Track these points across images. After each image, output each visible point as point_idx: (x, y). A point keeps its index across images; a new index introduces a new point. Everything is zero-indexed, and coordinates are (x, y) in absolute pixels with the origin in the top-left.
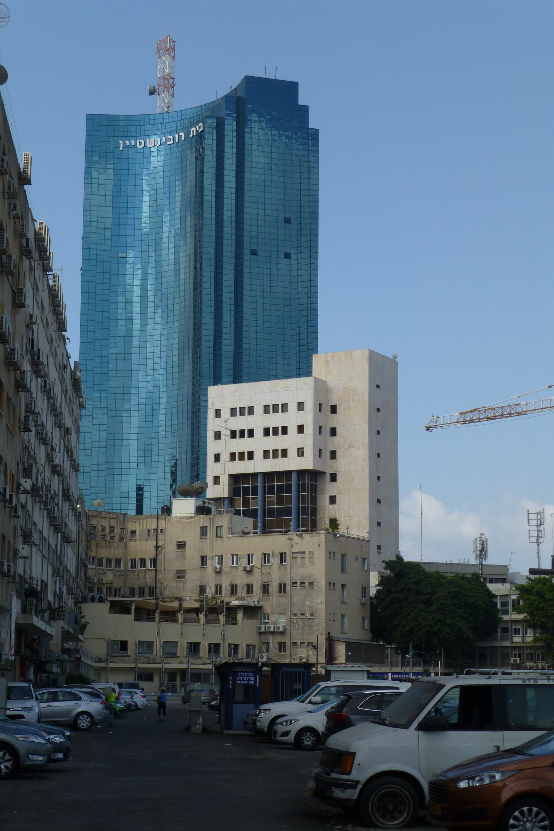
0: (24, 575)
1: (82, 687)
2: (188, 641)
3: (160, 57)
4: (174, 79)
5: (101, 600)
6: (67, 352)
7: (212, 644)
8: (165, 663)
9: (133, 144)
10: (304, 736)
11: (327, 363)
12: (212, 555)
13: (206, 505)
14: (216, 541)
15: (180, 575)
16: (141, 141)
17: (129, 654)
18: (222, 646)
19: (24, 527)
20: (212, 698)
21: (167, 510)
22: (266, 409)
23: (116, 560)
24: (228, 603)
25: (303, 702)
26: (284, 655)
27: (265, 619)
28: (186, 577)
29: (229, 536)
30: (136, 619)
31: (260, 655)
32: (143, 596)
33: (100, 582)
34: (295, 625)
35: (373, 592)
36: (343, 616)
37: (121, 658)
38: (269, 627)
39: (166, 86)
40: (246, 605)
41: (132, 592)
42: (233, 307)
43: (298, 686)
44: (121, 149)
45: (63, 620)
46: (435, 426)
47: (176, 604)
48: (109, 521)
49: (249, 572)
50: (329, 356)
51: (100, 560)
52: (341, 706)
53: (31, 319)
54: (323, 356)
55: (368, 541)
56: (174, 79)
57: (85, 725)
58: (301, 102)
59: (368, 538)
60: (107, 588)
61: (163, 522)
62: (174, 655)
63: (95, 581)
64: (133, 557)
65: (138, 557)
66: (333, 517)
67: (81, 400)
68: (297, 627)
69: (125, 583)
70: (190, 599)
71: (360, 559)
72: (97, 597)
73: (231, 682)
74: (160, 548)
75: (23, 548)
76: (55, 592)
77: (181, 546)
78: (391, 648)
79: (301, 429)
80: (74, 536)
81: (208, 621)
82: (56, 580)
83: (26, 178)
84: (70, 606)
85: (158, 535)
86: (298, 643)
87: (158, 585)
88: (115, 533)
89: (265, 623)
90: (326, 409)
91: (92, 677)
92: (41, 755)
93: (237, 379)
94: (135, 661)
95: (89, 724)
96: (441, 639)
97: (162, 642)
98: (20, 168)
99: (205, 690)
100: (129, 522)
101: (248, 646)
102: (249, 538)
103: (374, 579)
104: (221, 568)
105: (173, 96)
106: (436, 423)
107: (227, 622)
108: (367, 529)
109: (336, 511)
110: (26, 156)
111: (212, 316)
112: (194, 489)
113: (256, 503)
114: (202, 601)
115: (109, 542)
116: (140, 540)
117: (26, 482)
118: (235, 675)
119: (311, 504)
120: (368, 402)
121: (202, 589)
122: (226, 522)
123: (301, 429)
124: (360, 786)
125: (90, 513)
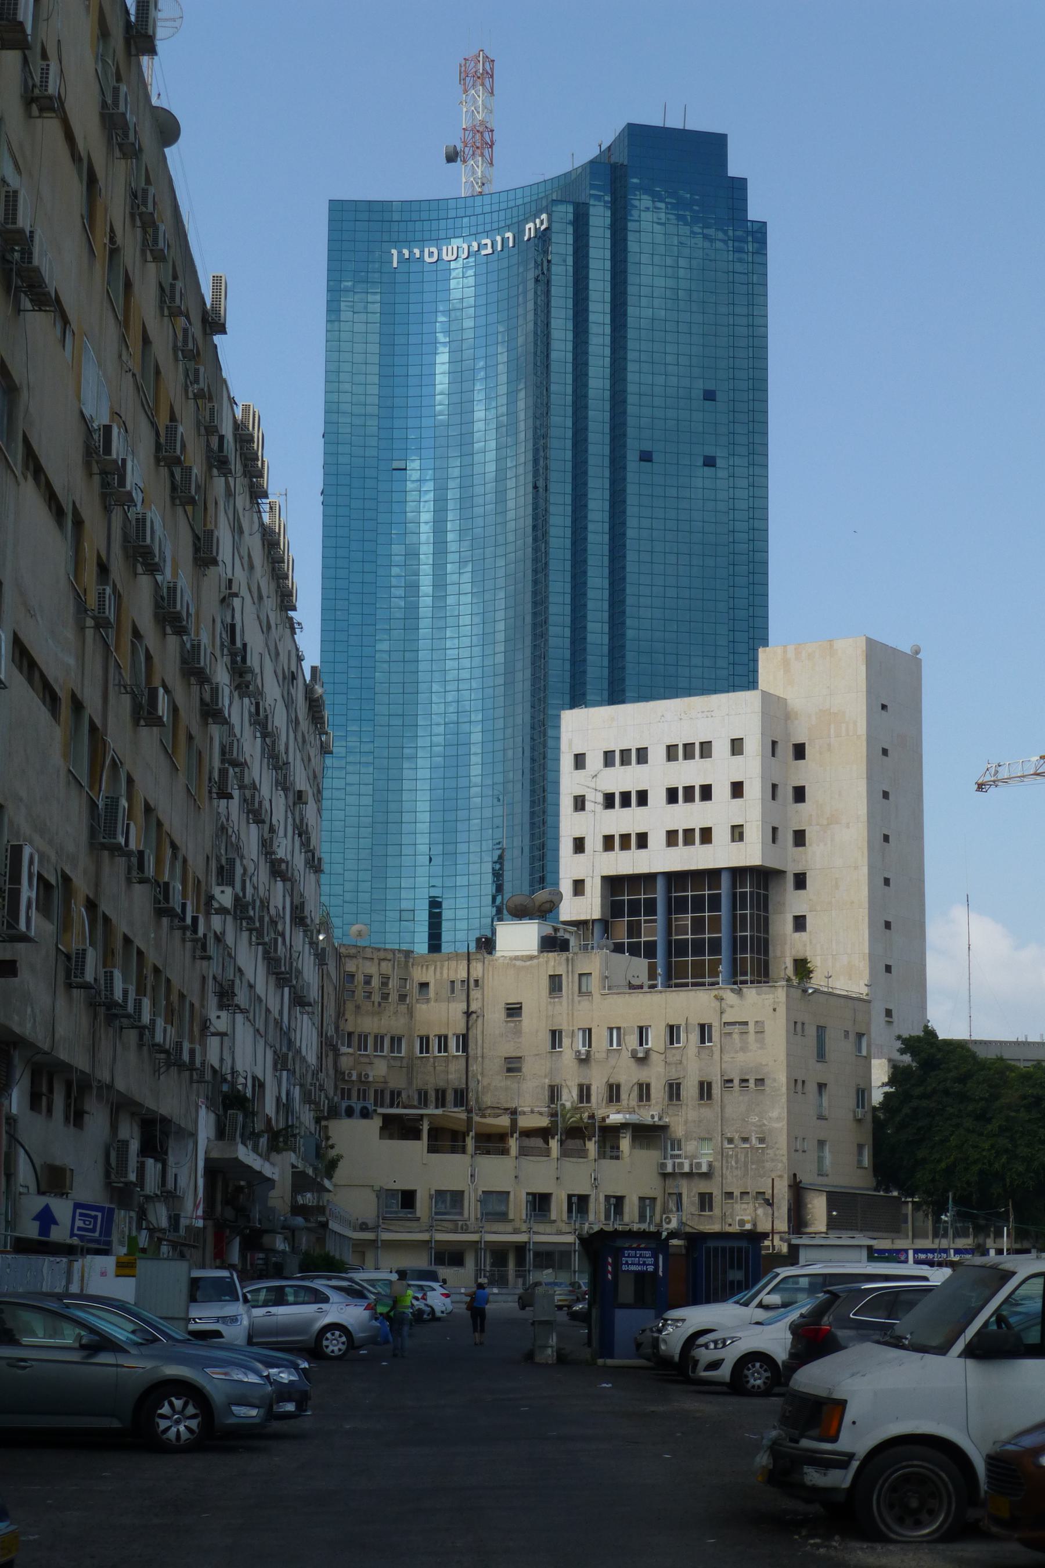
0: (221, 1067)
1: (329, 1278)
2: (530, 1191)
3: (466, 91)
4: (492, 131)
5: (365, 1114)
6: (297, 649)
7: (574, 1195)
8: (486, 1232)
9: (418, 256)
10: (749, 1369)
11: (786, 663)
12: (571, 1029)
13: (559, 934)
14: (579, 1002)
15: (513, 1066)
16: (432, 249)
17: (418, 1215)
18: (592, 1200)
19: (219, 978)
20: (575, 1298)
21: (487, 944)
22: (671, 752)
23: (392, 1039)
24: (604, 1119)
25: (746, 1304)
26: (710, 1217)
27: (673, 1149)
28: (524, 1070)
29: (603, 992)
30: (432, 1150)
31: (664, 1216)
32: (443, 1105)
33: (363, 1080)
34: (729, 1160)
35: (877, 1097)
36: (821, 1143)
37: (399, 1222)
38: (681, 1165)
39: (478, 145)
40: (637, 1122)
41: (423, 1098)
42: (606, 559)
43: (737, 1275)
44: (395, 265)
45: (294, 1152)
46: (994, 781)
47: (504, 1121)
48: (379, 964)
49: (642, 1061)
50: (791, 649)
51: (363, 1038)
52: (819, 1312)
53: (230, 588)
54: (779, 650)
55: (869, 1002)
56: (492, 131)
57: (336, 1349)
58: (731, 173)
59: (867, 995)
60: (376, 1091)
61: (479, 966)
62: (502, 1217)
63: (354, 1078)
64: (423, 1033)
65: (433, 1032)
66: (800, 956)
67: (324, 738)
68: (733, 1163)
69: (410, 1081)
70: (532, 1112)
71: (852, 1037)
72: (357, 1107)
73: (610, 1268)
74: (474, 1016)
75: (218, 1017)
76: (278, 1099)
77: (514, 1011)
78: (913, 1202)
79: (737, 789)
80: (314, 994)
81: (565, 1153)
82: (281, 1075)
83: (217, 323)
84: (307, 1124)
85: (471, 990)
86: (737, 1193)
87: (472, 1085)
88: (390, 986)
89: (673, 1157)
90: (786, 751)
91: (350, 1258)
92: (253, 1406)
93: (615, 696)
94: (430, 1229)
95: (343, 1347)
96: (1008, 1184)
97: (480, 1193)
98: (205, 304)
99: (561, 1284)
100: (415, 967)
101: (642, 1199)
102: (641, 995)
103: (880, 1073)
104: (588, 1053)
105: (491, 164)
106: (994, 775)
107: (602, 1155)
108: (866, 979)
109: (805, 945)
110: (217, 280)
111: (568, 579)
112: (537, 904)
113: (654, 931)
114: (554, 1115)
115: (380, 1004)
116: (436, 1000)
117: (223, 892)
118: (618, 1253)
119: (759, 931)
120: (864, 738)
121: (554, 1093)
122: (598, 964)
123: (737, 789)
124: (855, 1464)
125: (343, 950)
